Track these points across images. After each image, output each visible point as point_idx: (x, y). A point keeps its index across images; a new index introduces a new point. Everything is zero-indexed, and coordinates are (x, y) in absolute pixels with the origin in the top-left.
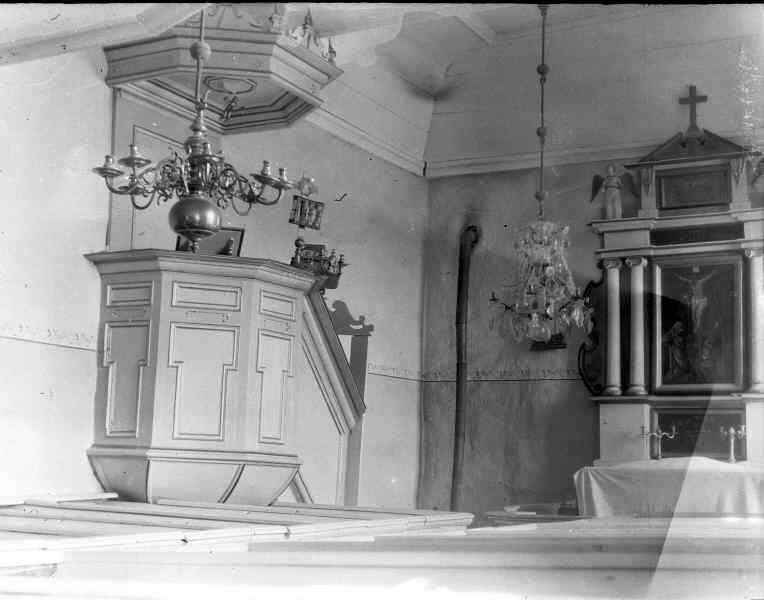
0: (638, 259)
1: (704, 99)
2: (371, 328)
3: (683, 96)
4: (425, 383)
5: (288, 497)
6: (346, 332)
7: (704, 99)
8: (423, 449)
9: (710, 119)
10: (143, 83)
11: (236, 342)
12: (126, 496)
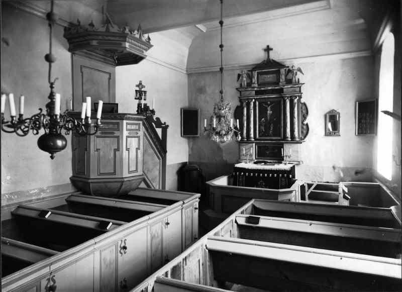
0: (296, 97)
1: (272, 49)
2: (168, 126)
3: (270, 47)
5: (143, 185)
7: (272, 49)
9: (273, 56)
10: (85, 51)
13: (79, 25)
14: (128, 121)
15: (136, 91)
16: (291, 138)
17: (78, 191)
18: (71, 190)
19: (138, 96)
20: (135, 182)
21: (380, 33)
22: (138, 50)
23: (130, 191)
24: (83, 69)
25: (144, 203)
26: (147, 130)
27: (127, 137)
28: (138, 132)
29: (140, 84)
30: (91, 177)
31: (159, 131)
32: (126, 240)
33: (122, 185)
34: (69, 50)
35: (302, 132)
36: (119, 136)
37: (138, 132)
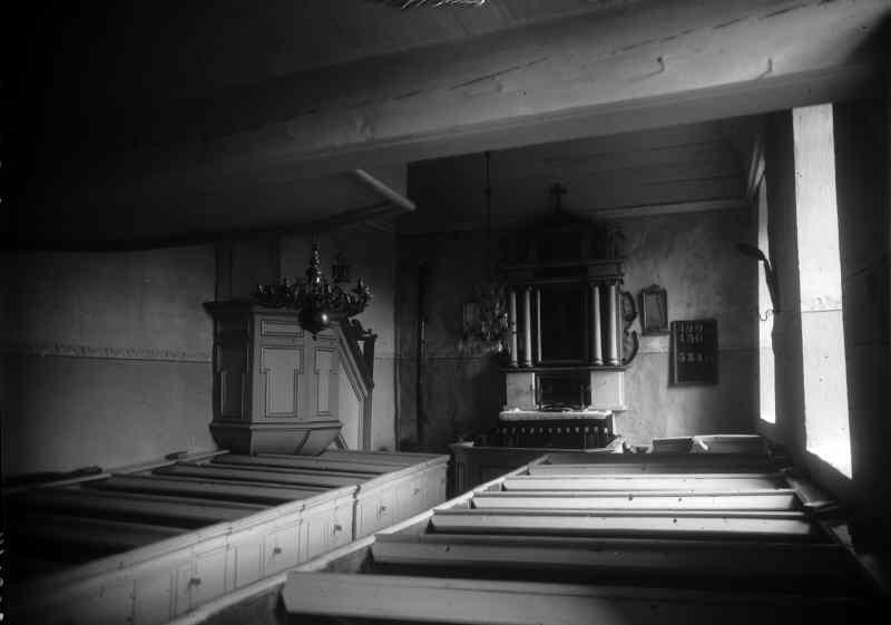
1: (564, 192)
2: (376, 336)
4: (395, 359)
5: (333, 446)
6: (362, 339)
8: (398, 384)
11: (302, 356)
12: (234, 452)
15: (334, 267)
16: (603, 360)
21: (753, 168)
35: (625, 349)
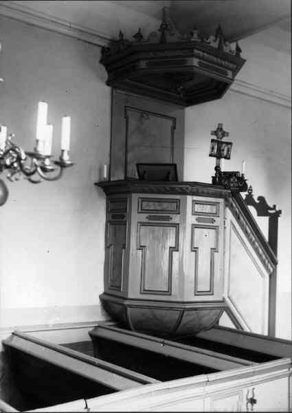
2: (280, 212)
10: (127, 80)
13: (122, 39)
14: (196, 198)
15: (213, 141)
17: (110, 321)
18: (99, 317)
19: (215, 151)
20: (208, 314)
22: (217, 70)
23: (198, 332)
24: (129, 113)
25: (230, 357)
26: (238, 219)
27: (194, 226)
28: (215, 218)
29: (220, 129)
30: (130, 296)
31: (263, 223)
32: (253, 389)
33: (182, 316)
34: (108, 83)
36: (178, 224)
37: (215, 218)
